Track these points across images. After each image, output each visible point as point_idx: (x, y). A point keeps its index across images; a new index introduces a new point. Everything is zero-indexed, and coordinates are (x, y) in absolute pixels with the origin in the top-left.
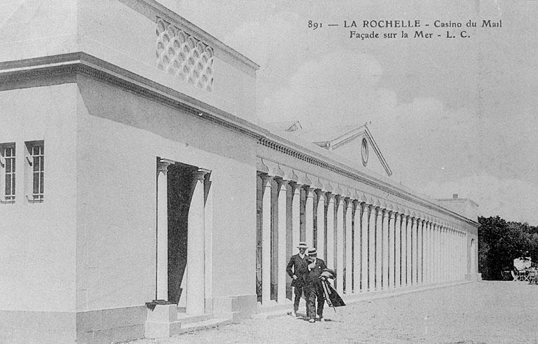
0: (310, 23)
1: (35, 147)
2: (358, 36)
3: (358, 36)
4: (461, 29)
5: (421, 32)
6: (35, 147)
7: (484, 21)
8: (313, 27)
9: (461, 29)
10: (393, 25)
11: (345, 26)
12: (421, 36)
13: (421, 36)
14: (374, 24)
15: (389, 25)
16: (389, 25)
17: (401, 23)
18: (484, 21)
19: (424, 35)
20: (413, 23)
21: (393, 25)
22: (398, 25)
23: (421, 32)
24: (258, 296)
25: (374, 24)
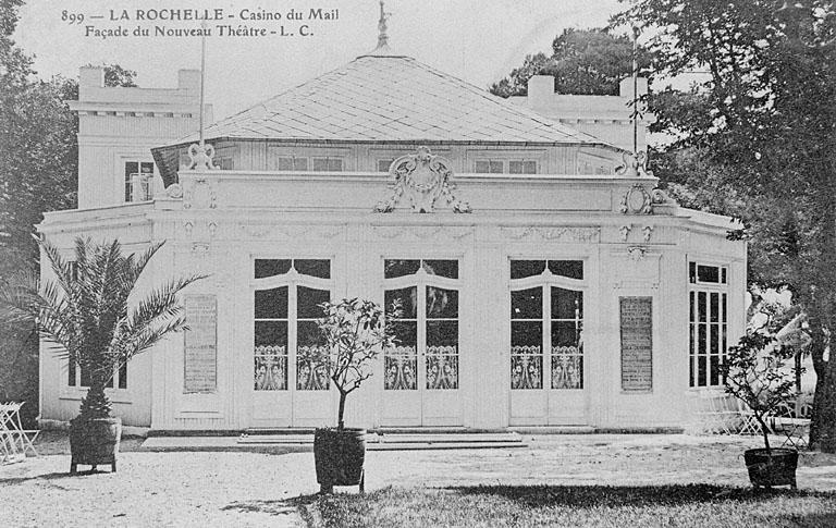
0: (65, 13)
1: (428, 388)
2: (98, 33)
3: (98, 33)
4: (301, 23)
5: (319, 11)
6: (387, 388)
7: (312, 10)
8: (69, 21)
9: (301, 23)
10: (182, 16)
11: (112, 19)
12: (318, 16)
13: (318, 16)
14: (152, 15)
15: (175, 17)
16: (175, 17)
17: (193, 13)
18: (312, 10)
19: (323, 17)
20: (212, 14)
21: (182, 16)
22: (188, 17)
23: (319, 11)
24: (817, 492)
25: (152, 15)
